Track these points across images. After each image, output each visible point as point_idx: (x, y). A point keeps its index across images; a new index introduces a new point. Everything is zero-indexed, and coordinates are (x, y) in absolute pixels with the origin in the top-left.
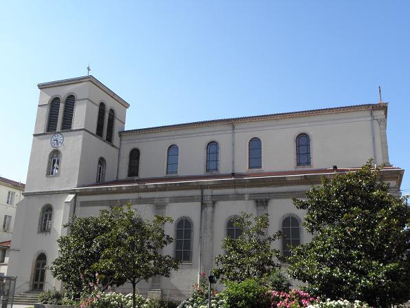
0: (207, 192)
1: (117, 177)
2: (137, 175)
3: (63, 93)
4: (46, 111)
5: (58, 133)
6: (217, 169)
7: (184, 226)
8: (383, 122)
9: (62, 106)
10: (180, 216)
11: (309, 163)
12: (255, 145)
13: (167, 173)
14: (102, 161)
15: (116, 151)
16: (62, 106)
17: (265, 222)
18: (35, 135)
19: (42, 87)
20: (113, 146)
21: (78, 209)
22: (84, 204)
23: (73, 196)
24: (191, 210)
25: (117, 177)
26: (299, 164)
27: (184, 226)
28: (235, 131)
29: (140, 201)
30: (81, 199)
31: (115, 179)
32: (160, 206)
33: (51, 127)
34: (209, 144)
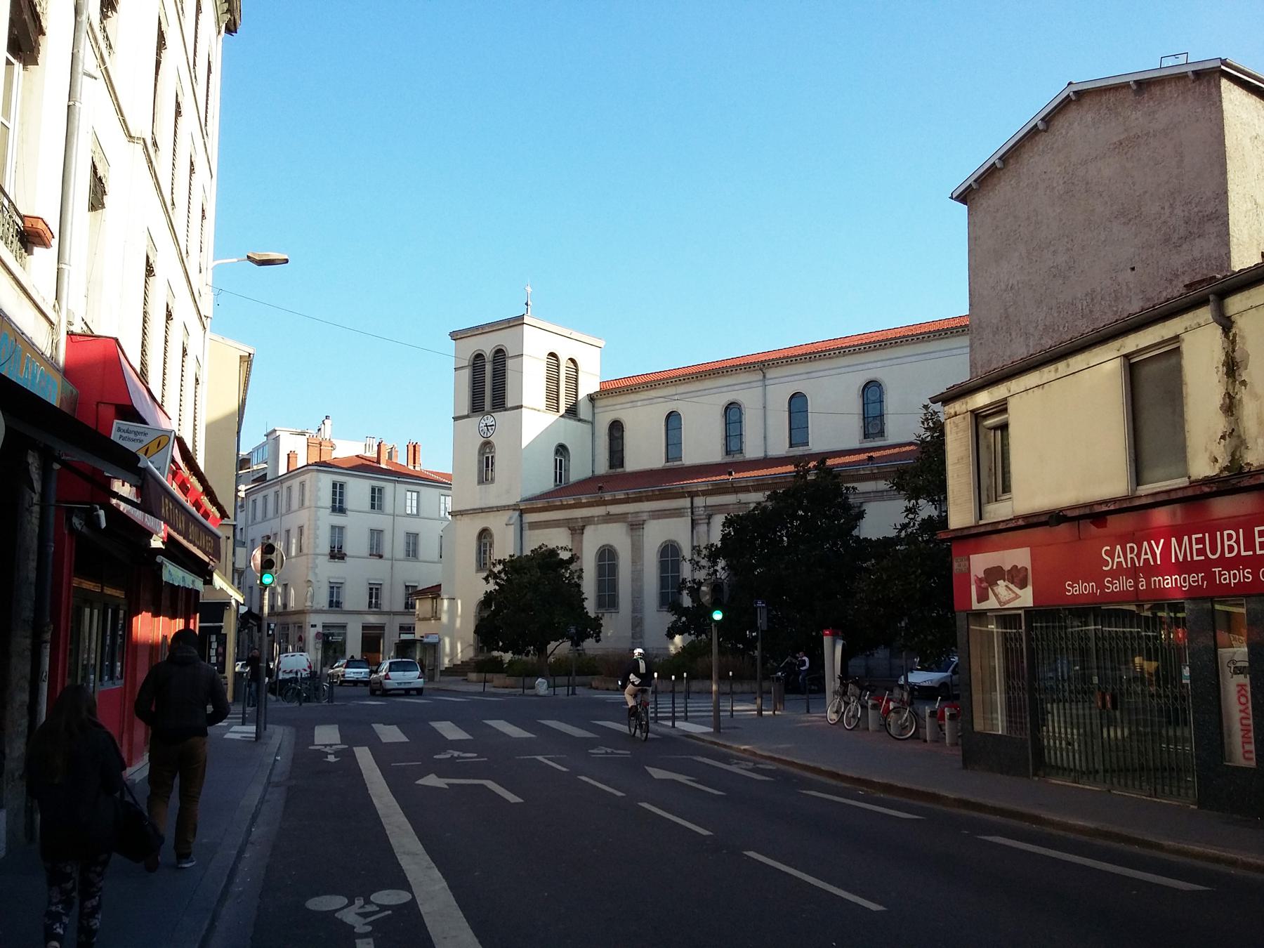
0: (699, 501)
1: (1227, 325)
2: (622, 465)
3: (487, 345)
4: (466, 374)
5: (488, 413)
6: (741, 451)
7: (607, 557)
8: (332, 548)
9: (488, 368)
10: (606, 542)
11: (881, 433)
12: (798, 404)
13: (667, 461)
14: (561, 450)
15: (587, 427)
16: (488, 368)
17: (637, 549)
18: (456, 419)
19: (456, 336)
20: (580, 420)
21: (527, 533)
22: (535, 526)
23: (1102, 371)
24: (616, 535)
25: (1227, 325)
26: (866, 436)
27: (607, 557)
28: (767, 382)
29: (609, 518)
30: (530, 518)
31: (590, 474)
32: (636, 526)
33: (477, 407)
34: (727, 408)
